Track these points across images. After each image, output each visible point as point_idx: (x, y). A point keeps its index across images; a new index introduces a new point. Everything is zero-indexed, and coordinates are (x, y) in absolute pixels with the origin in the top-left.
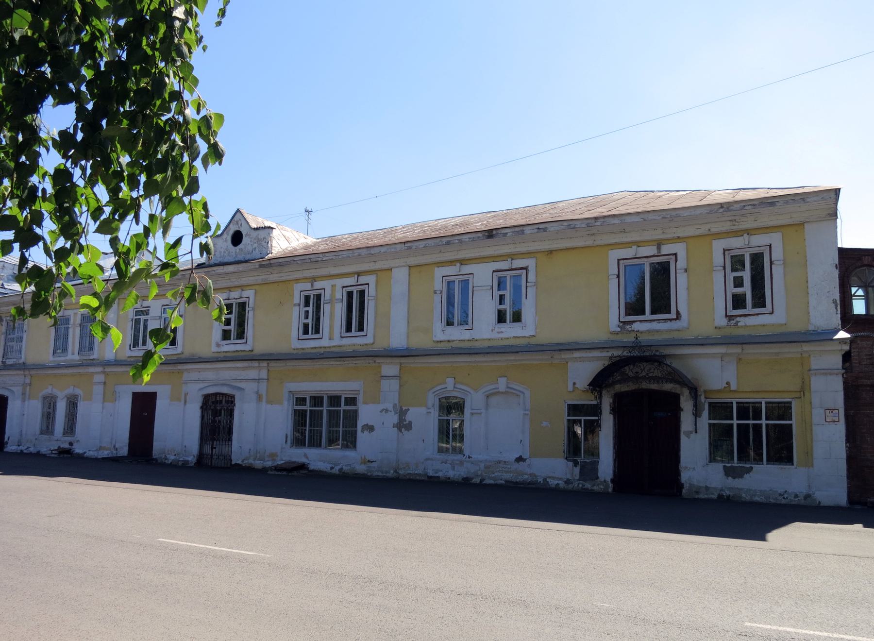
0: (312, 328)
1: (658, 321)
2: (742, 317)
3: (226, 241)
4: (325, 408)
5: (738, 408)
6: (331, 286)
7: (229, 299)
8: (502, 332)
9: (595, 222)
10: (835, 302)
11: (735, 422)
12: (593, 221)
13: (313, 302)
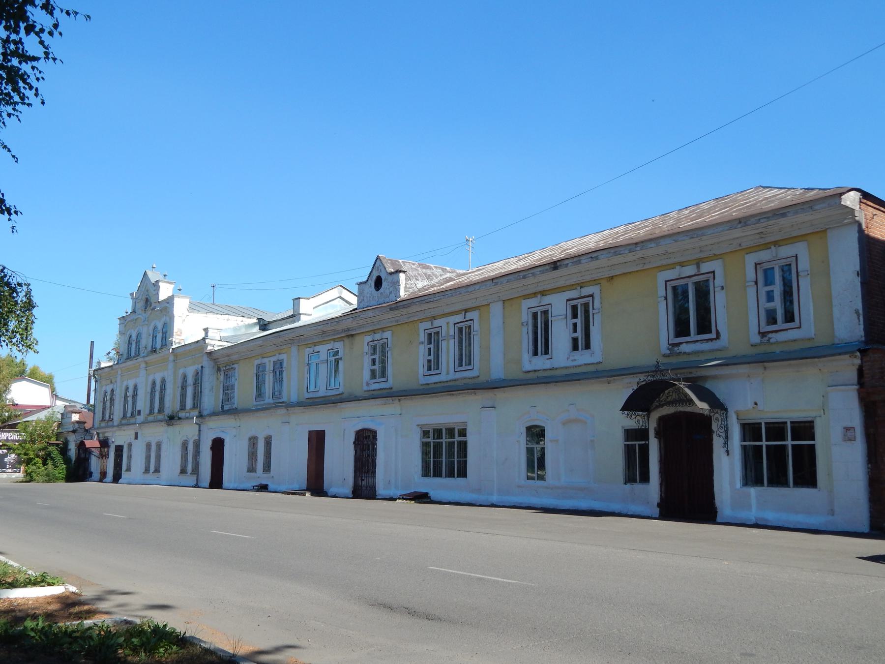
0: (433, 364)
1: (701, 342)
2: (774, 333)
3: (371, 287)
4: (444, 440)
5: (792, 428)
6: (446, 324)
7: (374, 341)
8: (575, 360)
9: (636, 247)
10: (857, 312)
11: (789, 443)
12: (634, 246)
13: (434, 338)
